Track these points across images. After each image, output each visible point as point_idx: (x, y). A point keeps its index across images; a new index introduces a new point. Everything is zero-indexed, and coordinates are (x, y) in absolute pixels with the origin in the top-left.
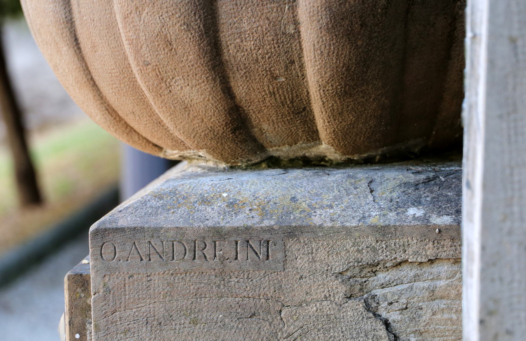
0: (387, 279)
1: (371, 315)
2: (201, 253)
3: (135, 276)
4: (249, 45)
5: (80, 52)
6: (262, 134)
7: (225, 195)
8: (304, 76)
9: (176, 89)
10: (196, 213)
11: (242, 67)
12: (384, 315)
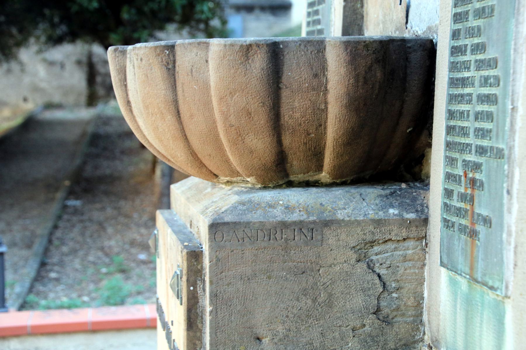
0: (379, 250)
1: (371, 271)
2: (274, 237)
3: (235, 251)
4: (298, 115)
5: (180, 119)
6: (291, 166)
7: (281, 202)
8: (325, 133)
9: (248, 140)
10: (268, 214)
11: (291, 128)
12: (378, 271)
